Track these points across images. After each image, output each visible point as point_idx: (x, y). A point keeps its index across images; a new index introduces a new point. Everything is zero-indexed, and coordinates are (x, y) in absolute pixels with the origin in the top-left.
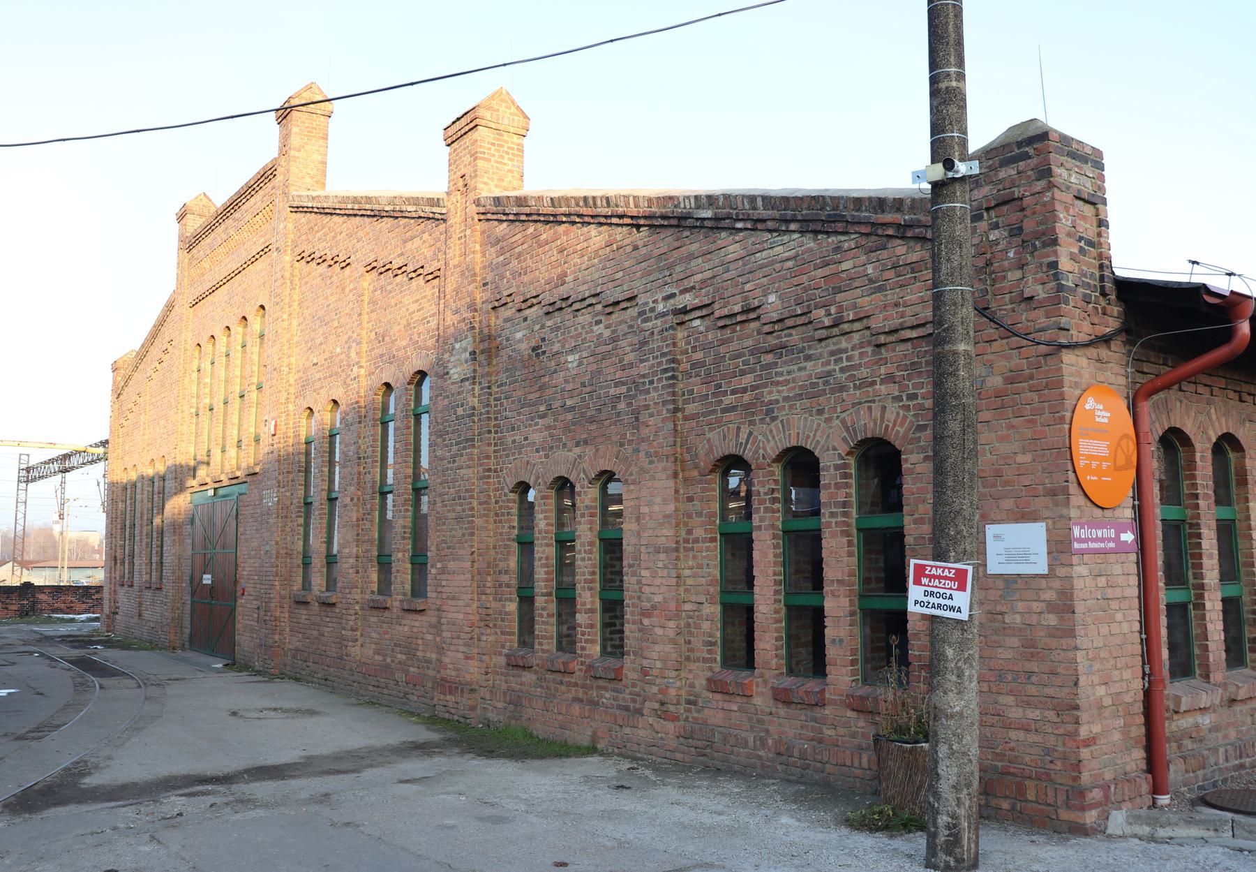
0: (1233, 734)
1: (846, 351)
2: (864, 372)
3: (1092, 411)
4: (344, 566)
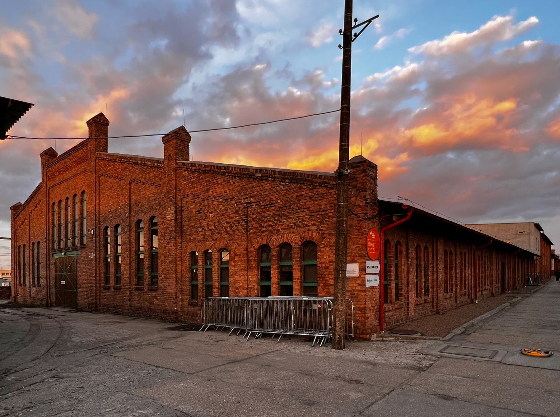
0: (395, 317)
2: (306, 223)
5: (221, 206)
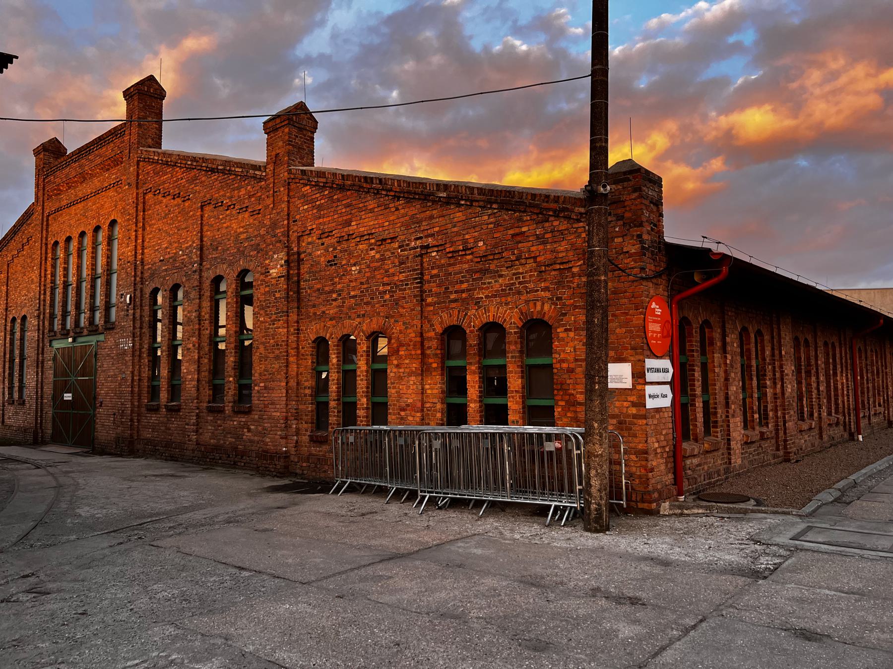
1: (522, 273)
2: (531, 286)
3: (654, 309)
4: (188, 386)
5: (372, 253)
